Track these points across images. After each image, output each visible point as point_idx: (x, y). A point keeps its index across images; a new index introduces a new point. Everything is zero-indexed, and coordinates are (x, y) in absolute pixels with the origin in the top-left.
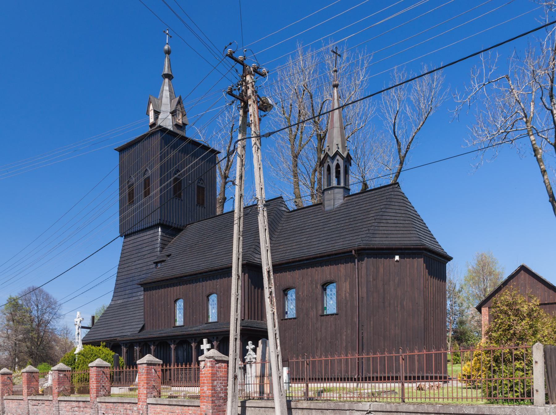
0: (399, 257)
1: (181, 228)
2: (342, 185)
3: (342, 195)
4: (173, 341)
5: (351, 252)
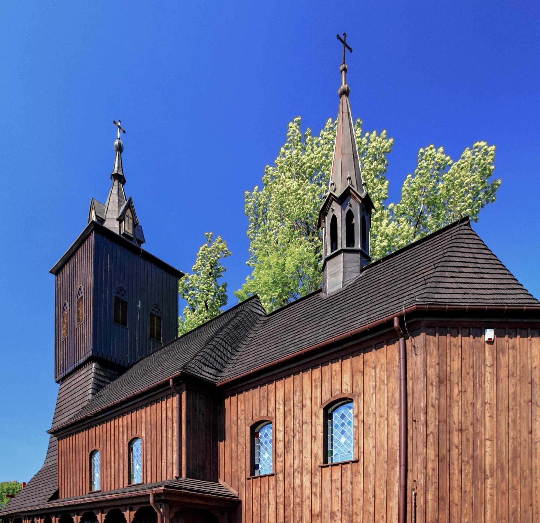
0: (495, 334)
1: (126, 365)
2: (358, 246)
3: (358, 263)
4: (76, 513)
5: (391, 321)
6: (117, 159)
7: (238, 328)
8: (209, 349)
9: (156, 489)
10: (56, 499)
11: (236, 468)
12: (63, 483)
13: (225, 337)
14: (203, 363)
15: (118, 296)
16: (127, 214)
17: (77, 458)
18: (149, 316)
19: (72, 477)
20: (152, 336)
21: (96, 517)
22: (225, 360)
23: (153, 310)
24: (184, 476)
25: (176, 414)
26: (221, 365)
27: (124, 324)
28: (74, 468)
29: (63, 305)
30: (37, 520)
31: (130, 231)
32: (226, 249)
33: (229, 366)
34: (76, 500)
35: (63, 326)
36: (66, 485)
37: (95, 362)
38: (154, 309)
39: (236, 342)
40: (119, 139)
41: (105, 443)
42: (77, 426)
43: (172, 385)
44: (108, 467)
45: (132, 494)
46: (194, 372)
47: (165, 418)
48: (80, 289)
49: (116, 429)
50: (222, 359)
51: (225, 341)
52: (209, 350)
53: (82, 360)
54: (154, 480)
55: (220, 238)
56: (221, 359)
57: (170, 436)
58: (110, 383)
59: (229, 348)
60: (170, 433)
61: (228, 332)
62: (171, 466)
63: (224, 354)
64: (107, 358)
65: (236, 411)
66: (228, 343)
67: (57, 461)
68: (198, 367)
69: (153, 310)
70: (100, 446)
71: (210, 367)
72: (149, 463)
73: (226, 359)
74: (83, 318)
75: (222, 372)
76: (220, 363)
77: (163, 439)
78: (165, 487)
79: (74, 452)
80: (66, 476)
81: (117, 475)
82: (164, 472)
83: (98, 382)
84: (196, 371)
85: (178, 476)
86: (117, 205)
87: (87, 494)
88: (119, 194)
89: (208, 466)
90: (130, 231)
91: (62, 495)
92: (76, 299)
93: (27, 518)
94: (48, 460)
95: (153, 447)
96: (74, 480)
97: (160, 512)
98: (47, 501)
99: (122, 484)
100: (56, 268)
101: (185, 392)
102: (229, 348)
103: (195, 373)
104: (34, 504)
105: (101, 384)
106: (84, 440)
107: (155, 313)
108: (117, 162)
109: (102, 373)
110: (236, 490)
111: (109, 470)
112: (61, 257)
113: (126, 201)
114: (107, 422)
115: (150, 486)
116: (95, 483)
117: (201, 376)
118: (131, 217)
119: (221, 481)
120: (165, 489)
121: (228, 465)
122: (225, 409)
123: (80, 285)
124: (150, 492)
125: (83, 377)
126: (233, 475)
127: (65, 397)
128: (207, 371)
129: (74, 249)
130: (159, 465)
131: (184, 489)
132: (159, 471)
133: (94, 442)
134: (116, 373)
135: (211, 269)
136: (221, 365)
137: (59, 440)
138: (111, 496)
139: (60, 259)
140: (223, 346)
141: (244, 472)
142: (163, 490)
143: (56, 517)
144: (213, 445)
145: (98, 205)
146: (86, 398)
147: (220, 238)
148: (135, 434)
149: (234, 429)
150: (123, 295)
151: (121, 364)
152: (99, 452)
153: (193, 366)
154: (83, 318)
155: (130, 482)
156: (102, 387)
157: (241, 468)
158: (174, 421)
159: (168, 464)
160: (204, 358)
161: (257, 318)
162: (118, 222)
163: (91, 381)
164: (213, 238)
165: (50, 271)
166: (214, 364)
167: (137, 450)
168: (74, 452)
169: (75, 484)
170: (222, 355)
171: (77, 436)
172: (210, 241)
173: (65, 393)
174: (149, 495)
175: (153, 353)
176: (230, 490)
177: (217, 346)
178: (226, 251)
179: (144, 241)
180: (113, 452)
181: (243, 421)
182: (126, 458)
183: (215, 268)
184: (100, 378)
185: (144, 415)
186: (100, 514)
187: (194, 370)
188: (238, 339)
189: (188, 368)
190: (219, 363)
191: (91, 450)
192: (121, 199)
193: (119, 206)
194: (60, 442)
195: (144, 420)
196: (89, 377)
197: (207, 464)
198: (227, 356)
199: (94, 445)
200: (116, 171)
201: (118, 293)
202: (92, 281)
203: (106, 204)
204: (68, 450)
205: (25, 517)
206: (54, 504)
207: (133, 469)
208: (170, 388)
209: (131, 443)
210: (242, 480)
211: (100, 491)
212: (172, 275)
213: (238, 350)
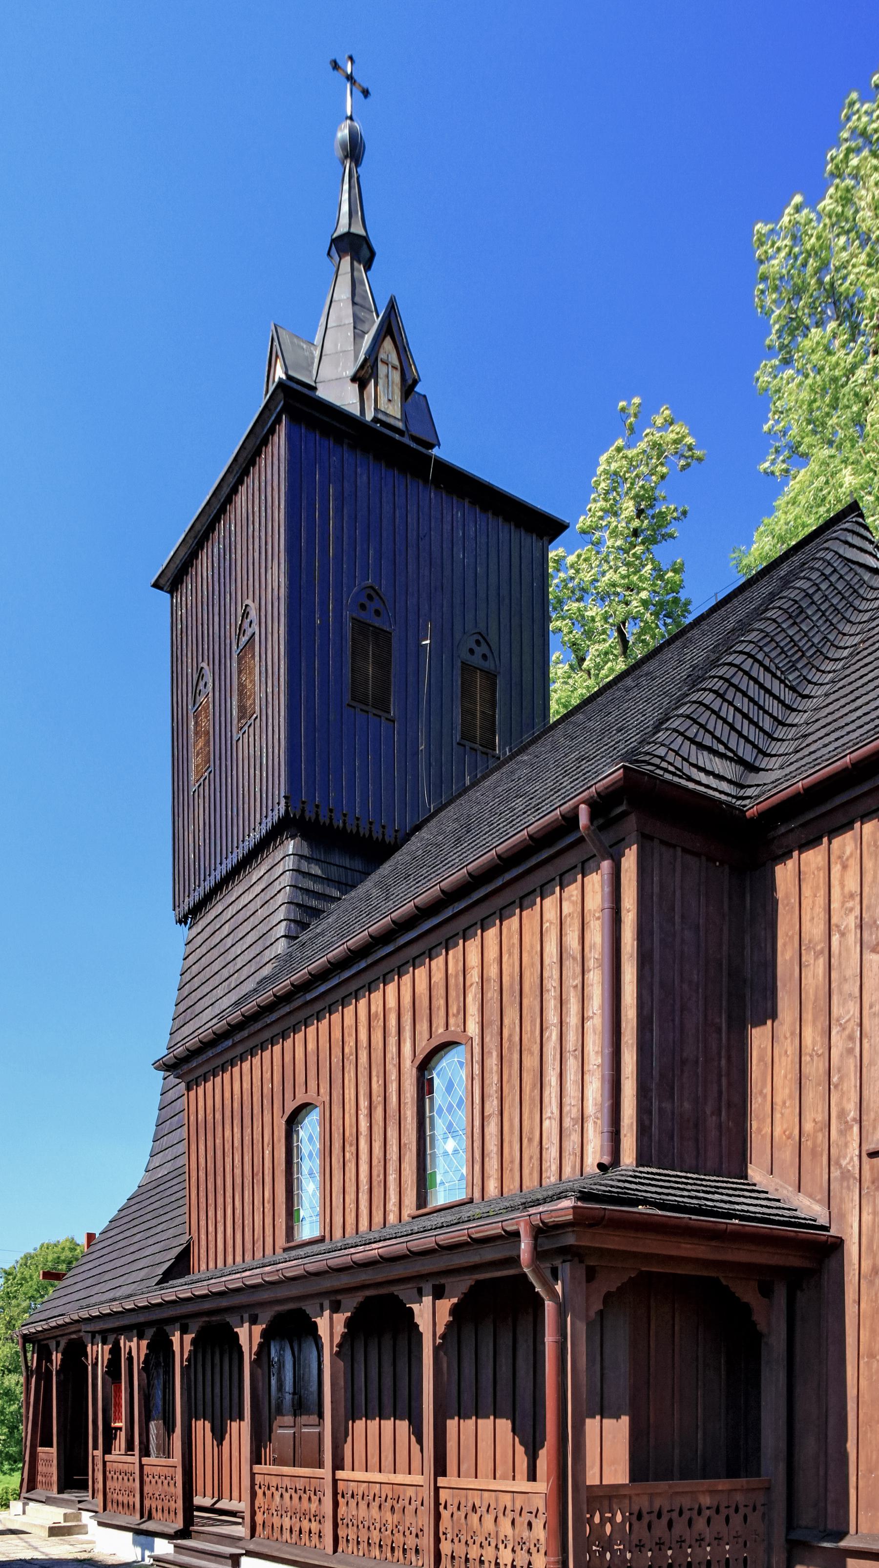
6: (346, 187)
7: (803, 616)
8: (711, 690)
9: (541, 1209)
10: (182, 1276)
11: (819, 1118)
12: (203, 1223)
13: (761, 649)
14: (692, 741)
15: (363, 616)
16: (382, 355)
17: (247, 1138)
18: (458, 672)
19: (229, 1200)
20: (467, 735)
21: (315, 1325)
22: (767, 727)
23: (472, 651)
24: (628, 1157)
25: (597, 935)
26: (755, 746)
27: (382, 704)
28: (238, 1171)
29: (195, 677)
30: (128, 1344)
31: (394, 410)
32: (689, 440)
33: (782, 748)
34: (248, 1273)
35: (196, 742)
36: (211, 1229)
37: (293, 837)
38: (474, 646)
39: (799, 666)
40: (351, 118)
41: (336, 1075)
42: (245, 1033)
43: (587, 828)
44: (347, 1155)
45: (427, 1242)
46: (666, 770)
47: (555, 958)
48: (246, 614)
49: (373, 1024)
50: (756, 725)
51: (761, 664)
52: (712, 696)
53: (255, 837)
54: (511, 1186)
55: (667, 412)
56: (752, 728)
57: (573, 1019)
58: (340, 899)
59: (776, 687)
60: (573, 1007)
61: (768, 630)
62: (578, 1127)
63: (761, 708)
64: (331, 819)
65: (821, 900)
66: (773, 668)
67: (183, 1160)
68: (677, 753)
69: (472, 651)
70: (322, 1091)
71: (716, 753)
72: (492, 1128)
73: (767, 723)
74: (258, 702)
75: (757, 770)
76: (751, 738)
77: (546, 1034)
78: (579, 1199)
79: (237, 1122)
80: (211, 1201)
81: (378, 1178)
82: (552, 1152)
83: (306, 898)
84: (671, 768)
85: (606, 1160)
86: (350, 334)
87: (279, 1250)
88: (357, 299)
89: (712, 1121)
90: (394, 410)
91: (201, 1264)
92: (234, 647)
93: (98, 1338)
94: (157, 1161)
95: (510, 1066)
96: (238, 1212)
97: (553, 1294)
98: (157, 1284)
99: (396, 1209)
100: (173, 566)
101: (634, 847)
102: (776, 687)
103: (668, 776)
104: (118, 1293)
105: (314, 903)
106: (267, 1076)
107: (476, 660)
108: (345, 196)
109: (316, 870)
110: (818, 1201)
111: (351, 1166)
112: (187, 530)
113: (378, 316)
114: (344, 1002)
115: (518, 1201)
116: (302, 1213)
117: (691, 785)
118: (396, 362)
119: (756, 1174)
120: (579, 1204)
121: (787, 1111)
122: (775, 902)
123: (246, 602)
124: (521, 1223)
125: (257, 889)
126: (807, 1144)
127: (204, 962)
128: (709, 768)
129: (226, 490)
130: (532, 1131)
131: (645, 1202)
132: (530, 1151)
133: (300, 1079)
134: (358, 865)
135: (638, 517)
136: (755, 746)
137: (189, 1089)
138: (368, 1247)
139: (183, 536)
140: (756, 681)
141: (856, 1129)
142: (574, 1208)
143: (184, 1331)
144: (728, 1039)
145: (292, 343)
146: (269, 954)
147: (667, 412)
148: (441, 1030)
149: (815, 970)
150: (377, 613)
151: (375, 836)
152: (318, 1109)
153: (662, 751)
154: (258, 702)
155: (422, 1200)
156: (316, 913)
157: (842, 1114)
158: (591, 963)
159: (567, 1123)
160: (695, 721)
161: (862, 581)
162: (356, 386)
163: (281, 898)
164: (644, 415)
165: (153, 581)
166: (732, 745)
167: (450, 1087)
168: (237, 1122)
169: (239, 1222)
170: (753, 712)
171: (246, 1065)
172: (632, 429)
173: (204, 949)
174: (517, 1234)
175: (474, 784)
176: (795, 1204)
177: (735, 681)
178: (690, 448)
179: (435, 442)
180: (364, 1104)
181: (852, 938)
182: (409, 1119)
183: (651, 512)
184: (310, 884)
185: (473, 959)
186: (327, 1313)
187: (664, 765)
188: (803, 655)
189: (647, 758)
190: (747, 740)
191: (290, 1107)
192: (362, 314)
193: (358, 335)
194: (192, 1094)
195: (474, 976)
196: (277, 886)
197: (708, 1112)
198: (771, 715)
199: (300, 1089)
200: (343, 228)
201: (363, 607)
202: (282, 580)
203: (318, 340)
204: (218, 1116)
205: (93, 1334)
206: (179, 1289)
207: (433, 1155)
208: (581, 840)
209: (425, 1066)
210: (844, 1163)
211: (322, 1240)
212: (529, 530)
213: (806, 692)
